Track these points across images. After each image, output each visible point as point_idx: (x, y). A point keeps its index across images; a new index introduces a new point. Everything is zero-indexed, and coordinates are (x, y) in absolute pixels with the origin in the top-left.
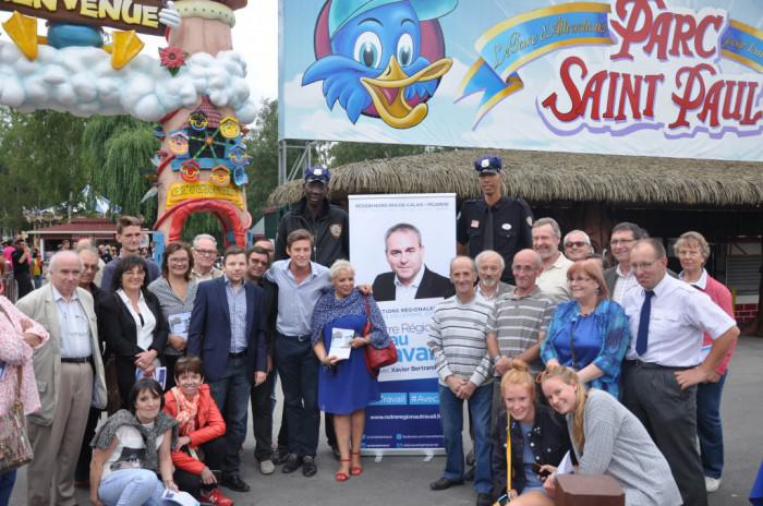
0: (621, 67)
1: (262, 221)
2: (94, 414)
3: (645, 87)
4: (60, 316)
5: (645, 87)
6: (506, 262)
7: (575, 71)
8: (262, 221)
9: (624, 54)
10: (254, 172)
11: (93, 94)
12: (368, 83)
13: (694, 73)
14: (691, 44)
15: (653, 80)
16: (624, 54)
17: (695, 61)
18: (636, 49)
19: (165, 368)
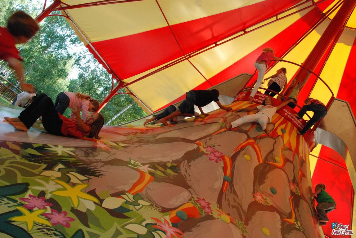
0: (339, 230)
1: (100, 153)
2: (192, 195)
3: (341, 232)
4: (174, 198)
5: (341, 232)
6: (250, 156)
7: (334, 231)
8: (100, 153)
9: (339, 229)
10: (94, 138)
11: (251, 113)
12: (45, 226)
13: (346, 230)
14: (345, 228)
15: (342, 231)
16: (339, 229)
17: (346, 229)
18: (340, 229)
19: (270, 205)
